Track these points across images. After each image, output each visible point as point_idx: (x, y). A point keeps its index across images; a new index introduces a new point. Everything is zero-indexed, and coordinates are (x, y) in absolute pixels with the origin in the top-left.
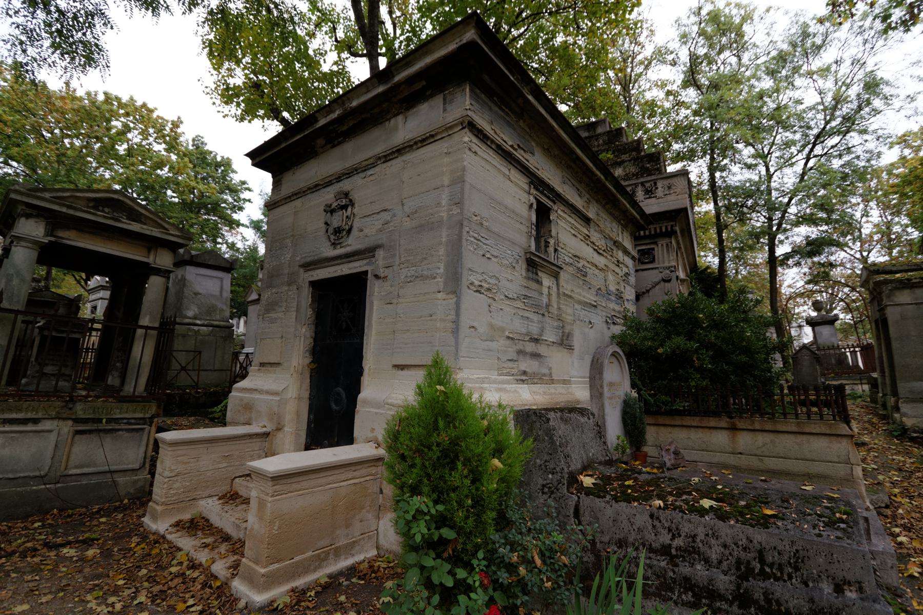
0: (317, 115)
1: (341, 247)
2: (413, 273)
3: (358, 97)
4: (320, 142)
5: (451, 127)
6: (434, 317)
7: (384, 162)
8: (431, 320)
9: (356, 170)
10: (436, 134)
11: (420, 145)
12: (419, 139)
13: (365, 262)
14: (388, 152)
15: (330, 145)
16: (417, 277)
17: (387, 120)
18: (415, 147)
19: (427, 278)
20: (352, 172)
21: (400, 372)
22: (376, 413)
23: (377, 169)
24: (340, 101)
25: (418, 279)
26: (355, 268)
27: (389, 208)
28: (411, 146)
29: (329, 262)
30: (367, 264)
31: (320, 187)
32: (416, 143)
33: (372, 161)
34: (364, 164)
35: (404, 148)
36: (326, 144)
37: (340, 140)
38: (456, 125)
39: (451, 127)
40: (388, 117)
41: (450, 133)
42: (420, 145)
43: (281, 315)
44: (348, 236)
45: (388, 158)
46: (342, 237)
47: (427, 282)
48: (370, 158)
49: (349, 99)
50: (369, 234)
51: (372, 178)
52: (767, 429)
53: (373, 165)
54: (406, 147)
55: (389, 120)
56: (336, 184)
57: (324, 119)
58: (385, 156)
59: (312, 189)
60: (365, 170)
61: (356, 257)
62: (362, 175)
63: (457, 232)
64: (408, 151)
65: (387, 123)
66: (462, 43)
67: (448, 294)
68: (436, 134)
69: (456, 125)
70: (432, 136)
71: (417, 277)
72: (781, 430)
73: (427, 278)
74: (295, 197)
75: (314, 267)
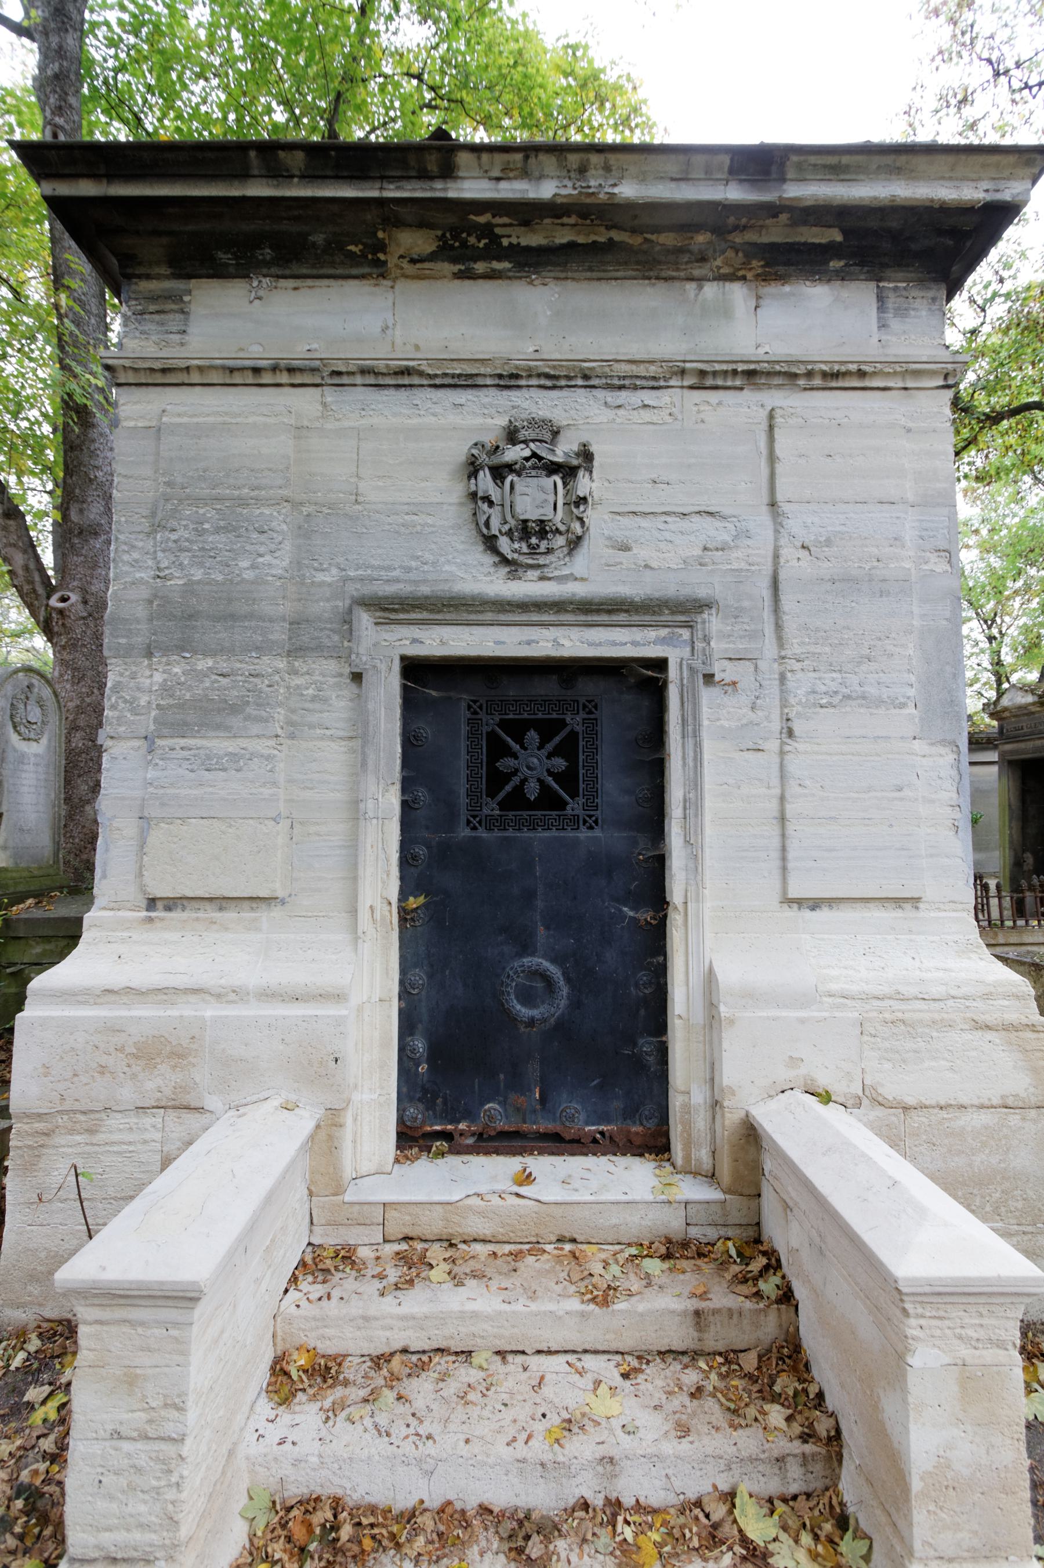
0: (463, 158)
1: (542, 578)
2: (833, 686)
3: (642, 178)
4: (421, 242)
5: (917, 374)
6: (907, 793)
7: (691, 387)
8: (902, 799)
9: (586, 377)
10: (874, 374)
11: (817, 382)
12: (824, 367)
13: (652, 634)
14: (718, 367)
15: (449, 268)
16: (848, 697)
17: (691, 279)
18: (802, 382)
19: (879, 702)
20: (568, 378)
21: (807, 914)
22: (802, 1021)
23: (664, 398)
24: (573, 159)
25: (854, 703)
26: (614, 644)
27: (726, 511)
28: (795, 376)
29: (504, 611)
30: (663, 641)
31: (416, 380)
32: (810, 374)
33: (653, 370)
34: (625, 369)
35: (769, 374)
36: (432, 257)
37: (497, 265)
38: (932, 373)
39: (917, 374)
40: (697, 273)
41: (909, 385)
42: (817, 382)
43: (262, 746)
44: (570, 553)
45: (709, 382)
46: (549, 551)
47: (882, 711)
48: (652, 362)
49: (607, 168)
50: (654, 564)
51: (646, 415)
52: (1012, 942)
53: (655, 384)
54: (779, 373)
55: (700, 280)
56: (493, 392)
57: (485, 184)
58: (703, 373)
59: (377, 374)
60: (621, 388)
61: (622, 617)
62: (611, 397)
63: (948, 614)
64: (779, 387)
65: (691, 287)
66: (998, 196)
67: (932, 744)
68: (874, 374)
69: (932, 373)
70: (861, 374)
71: (848, 697)
72: (1027, 941)
73: (879, 702)
74: (284, 378)
75: (425, 615)
